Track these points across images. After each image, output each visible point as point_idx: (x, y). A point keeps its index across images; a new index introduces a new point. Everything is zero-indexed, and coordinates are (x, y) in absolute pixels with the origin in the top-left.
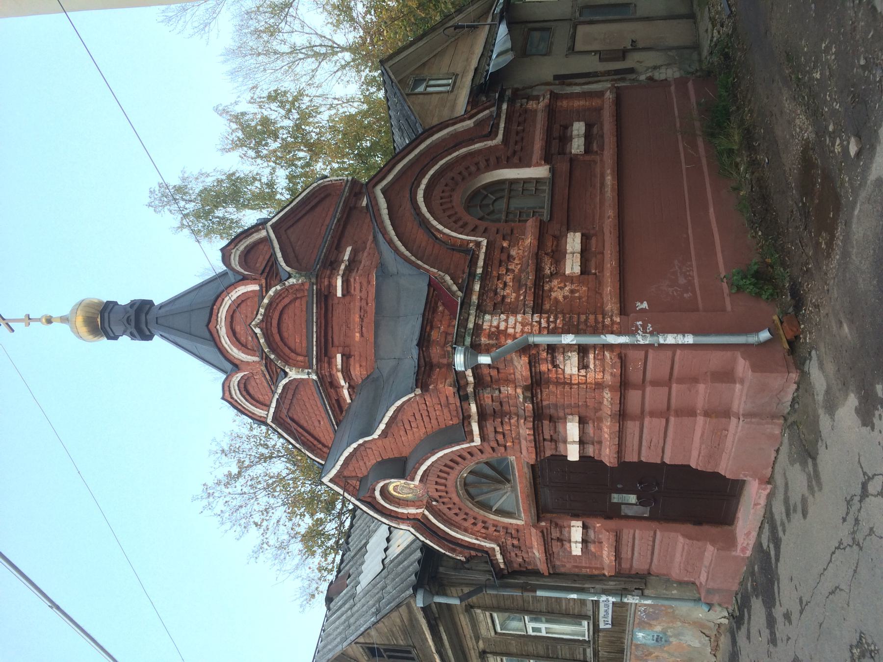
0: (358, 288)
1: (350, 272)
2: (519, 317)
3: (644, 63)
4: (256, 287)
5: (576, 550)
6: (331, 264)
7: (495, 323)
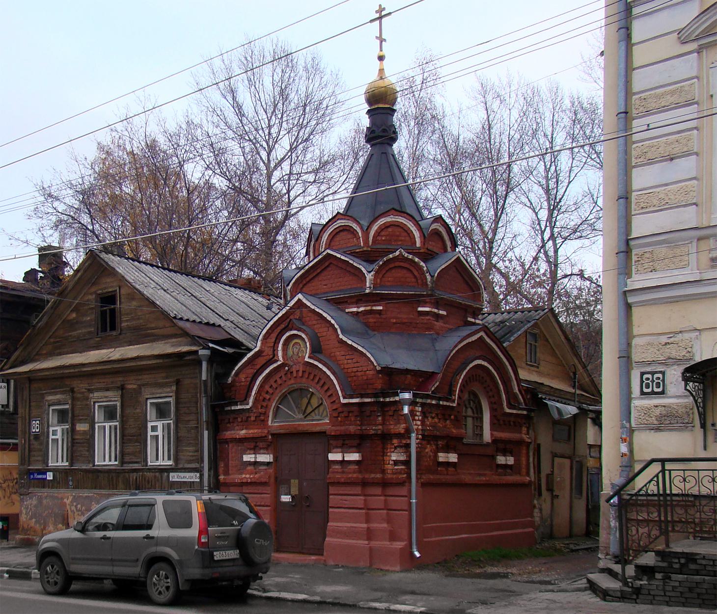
3: (544, 503)
4: (418, 245)
7: (418, 414)
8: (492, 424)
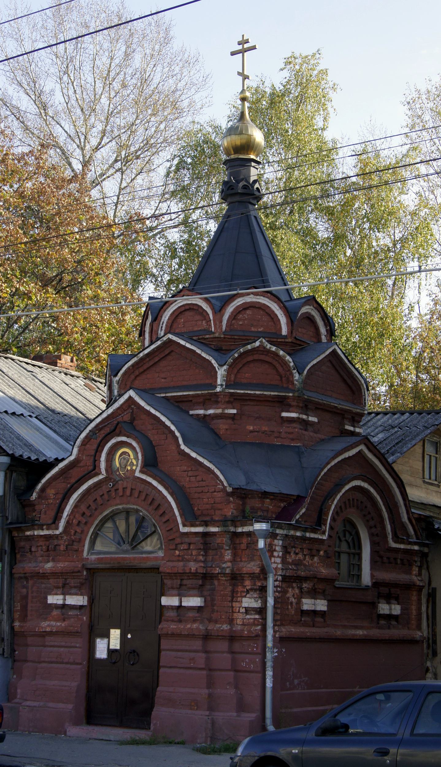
0: (290, 430)
1: (300, 423)
2: (280, 566)
4: (284, 331)
5: (54, 599)
6: (306, 406)
8: (373, 562)
